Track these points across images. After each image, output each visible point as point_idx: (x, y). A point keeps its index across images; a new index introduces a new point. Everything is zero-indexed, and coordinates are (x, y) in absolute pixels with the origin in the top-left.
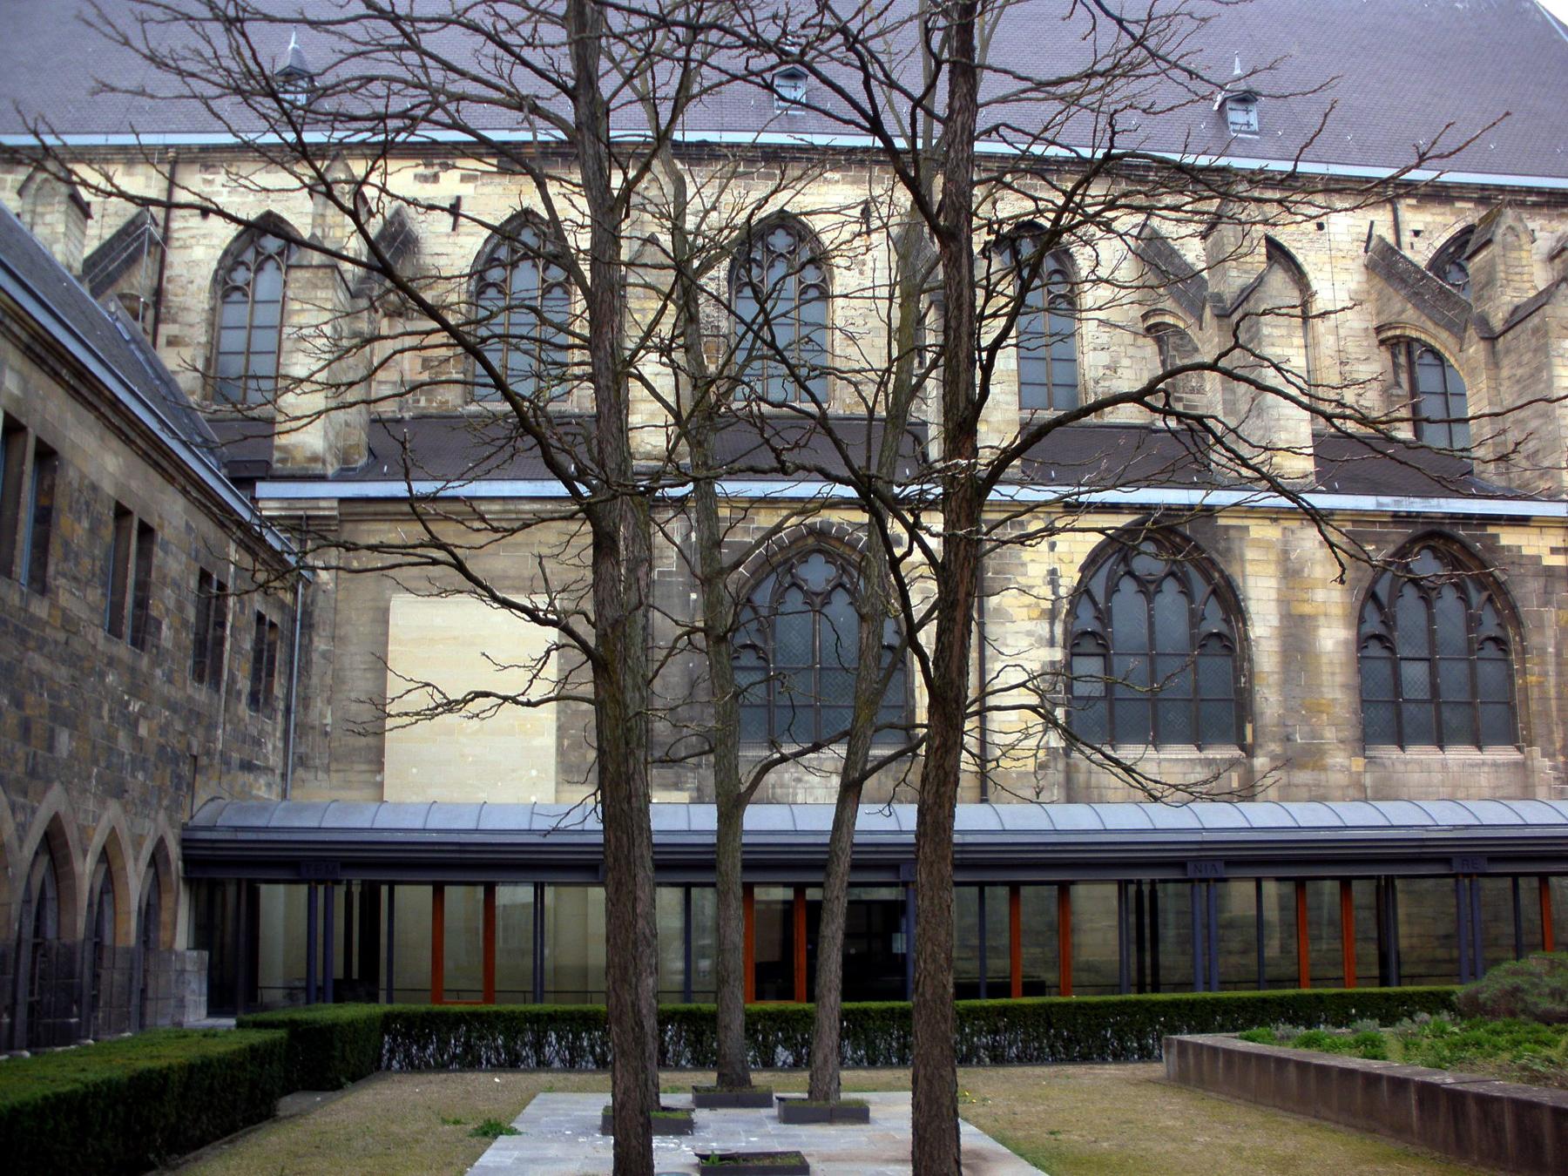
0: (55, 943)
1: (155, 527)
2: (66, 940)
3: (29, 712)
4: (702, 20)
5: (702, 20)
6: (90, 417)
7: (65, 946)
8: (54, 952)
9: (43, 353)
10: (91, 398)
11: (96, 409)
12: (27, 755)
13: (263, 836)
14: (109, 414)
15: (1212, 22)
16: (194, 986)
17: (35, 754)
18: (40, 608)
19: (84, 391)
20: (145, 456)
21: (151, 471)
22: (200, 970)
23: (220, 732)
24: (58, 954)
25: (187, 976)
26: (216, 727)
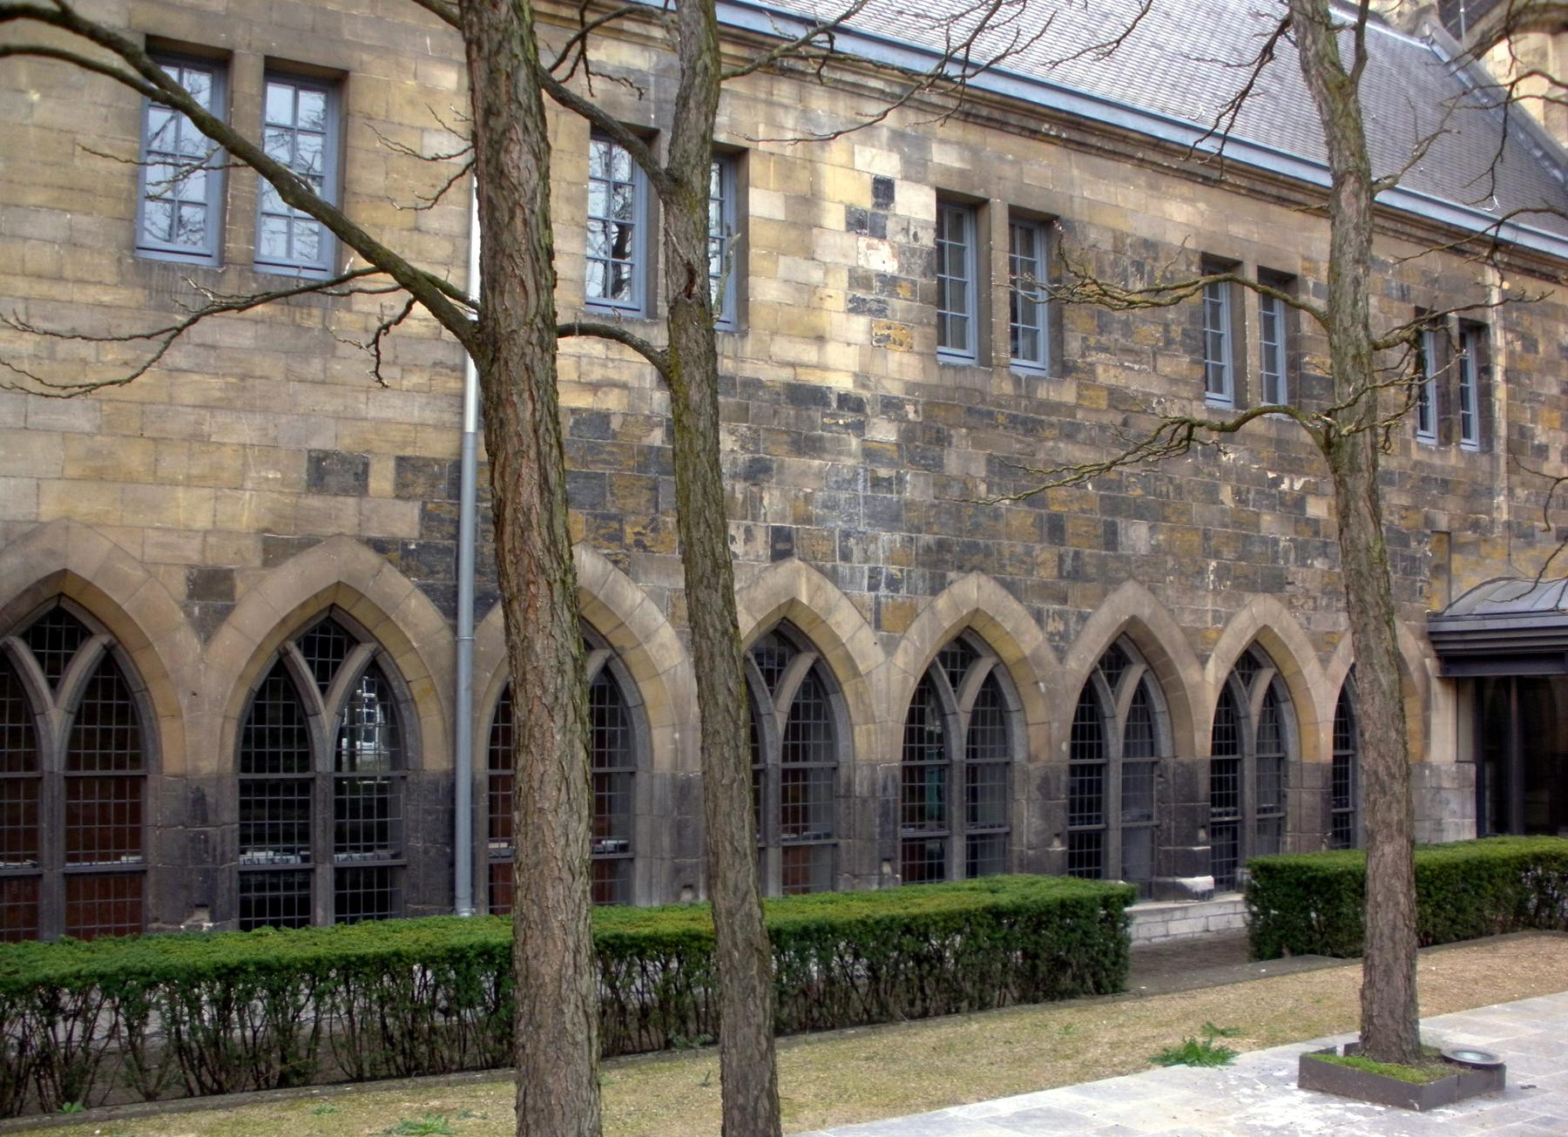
0: (1172, 763)
1: (54, 567)
2: (1185, 758)
3: (1055, 508)
4: (884, 107)
5: (884, 107)
6: (1127, 167)
7: (1181, 764)
8: (1171, 771)
9: (997, 114)
10: (1109, 146)
11: (1131, 157)
12: (1061, 558)
13: (1514, 623)
14: (1158, 158)
15: (387, 393)
16: (1454, 805)
17: (1077, 555)
18: (1067, 393)
19: (1093, 140)
20: (1252, 193)
21: (1275, 210)
22: (1461, 787)
23: (1501, 499)
24: (1174, 775)
25: (1444, 794)
26: (1490, 493)
